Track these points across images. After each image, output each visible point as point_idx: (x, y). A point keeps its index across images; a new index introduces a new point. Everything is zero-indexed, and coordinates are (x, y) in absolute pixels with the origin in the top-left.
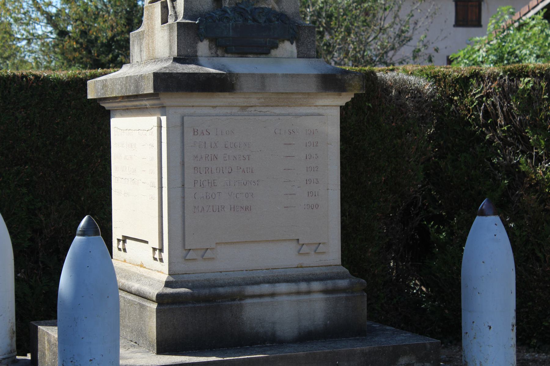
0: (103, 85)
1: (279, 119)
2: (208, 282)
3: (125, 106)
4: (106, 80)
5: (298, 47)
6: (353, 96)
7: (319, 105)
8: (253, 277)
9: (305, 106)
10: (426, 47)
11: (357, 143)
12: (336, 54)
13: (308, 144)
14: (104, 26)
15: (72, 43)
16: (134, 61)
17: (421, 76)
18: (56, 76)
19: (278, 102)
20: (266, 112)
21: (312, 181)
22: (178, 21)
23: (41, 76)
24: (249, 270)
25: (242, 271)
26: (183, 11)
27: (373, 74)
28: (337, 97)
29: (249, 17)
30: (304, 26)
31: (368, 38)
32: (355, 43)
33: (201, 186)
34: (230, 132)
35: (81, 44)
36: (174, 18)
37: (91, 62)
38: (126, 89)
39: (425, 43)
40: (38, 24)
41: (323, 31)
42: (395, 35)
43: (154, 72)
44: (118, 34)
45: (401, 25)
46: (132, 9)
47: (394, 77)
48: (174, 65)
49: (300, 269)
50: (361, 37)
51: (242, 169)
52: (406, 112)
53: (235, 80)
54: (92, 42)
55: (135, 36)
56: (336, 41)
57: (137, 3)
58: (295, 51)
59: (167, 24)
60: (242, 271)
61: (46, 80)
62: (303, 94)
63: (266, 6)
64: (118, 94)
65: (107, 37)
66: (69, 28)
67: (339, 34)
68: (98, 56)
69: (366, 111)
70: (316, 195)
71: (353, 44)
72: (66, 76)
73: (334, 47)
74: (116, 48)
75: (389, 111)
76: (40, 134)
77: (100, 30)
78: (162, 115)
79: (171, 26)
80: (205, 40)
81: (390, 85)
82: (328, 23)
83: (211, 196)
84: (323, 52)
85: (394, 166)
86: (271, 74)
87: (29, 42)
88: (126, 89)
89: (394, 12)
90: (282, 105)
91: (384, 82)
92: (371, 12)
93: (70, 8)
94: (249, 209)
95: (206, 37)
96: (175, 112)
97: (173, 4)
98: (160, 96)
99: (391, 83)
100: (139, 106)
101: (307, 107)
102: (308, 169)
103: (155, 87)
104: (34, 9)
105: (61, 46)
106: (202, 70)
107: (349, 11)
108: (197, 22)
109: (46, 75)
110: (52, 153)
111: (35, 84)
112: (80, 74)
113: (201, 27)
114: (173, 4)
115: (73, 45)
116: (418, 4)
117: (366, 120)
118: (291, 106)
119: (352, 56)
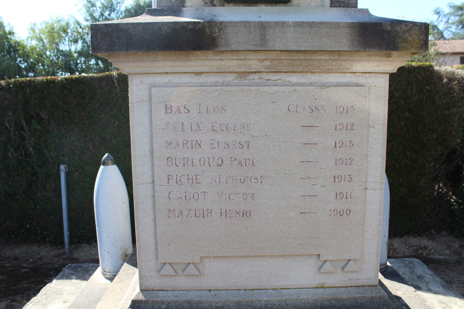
1: (296, 91)
2: (189, 305)
7: (357, 71)
8: (252, 301)
9: (336, 73)
11: (418, 113)
13: (338, 127)
19: (293, 65)
20: (277, 80)
21: (343, 178)
24: (249, 290)
25: (239, 290)
28: (384, 59)
33: (177, 183)
34: (220, 109)
49: (321, 290)
51: (238, 160)
52: (453, 94)
53: (217, 31)
60: (239, 290)
69: (425, 92)
70: (348, 197)
83: (192, 197)
85: (442, 128)
86: (276, 22)
90: (300, 70)
94: (248, 215)
96: (141, 82)
101: (339, 74)
102: (338, 162)
117: (425, 98)
118: (315, 73)
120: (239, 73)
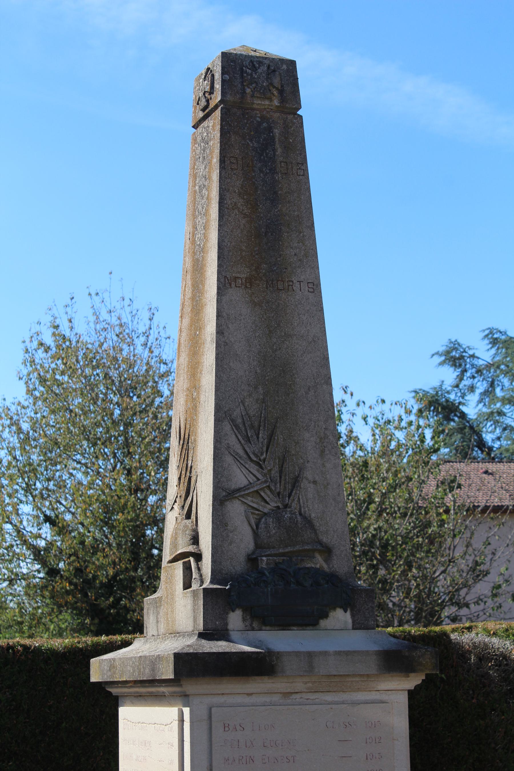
0: (111, 665)
3: (137, 693)
4: (114, 660)
5: (353, 616)
6: (424, 678)
10: (508, 583)
12: (394, 593)
13: (368, 740)
14: (104, 562)
15: (65, 583)
16: (148, 634)
17: (506, 638)
18: (49, 646)
19: (330, 686)
22: (204, 586)
23: (31, 646)
26: (210, 574)
27: (446, 637)
28: (404, 679)
29: (292, 580)
30: (360, 590)
31: (435, 572)
32: (418, 580)
35: (76, 585)
36: (199, 582)
37: (87, 608)
38: (140, 671)
39: (506, 577)
40: (23, 561)
41: (377, 564)
42: (469, 568)
43: (174, 652)
44: (122, 572)
45: (476, 556)
46: (138, 540)
47: (472, 640)
48: (200, 642)
50: (425, 572)
53: (275, 660)
54: (89, 583)
55: (150, 603)
56: (394, 577)
57: (145, 533)
58: (350, 621)
59: (191, 589)
61: (38, 650)
62: (361, 676)
63: (313, 566)
64: (129, 677)
65: (107, 575)
66: (61, 565)
67: (397, 568)
68: (96, 600)
71: (415, 580)
72: (61, 646)
73: (392, 584)
74: (118, 589)
75: (468, 684)
76: (28, 720)
77: (101, 567)
78: (185, 706)
79: (196, 593)
80: (237, 609)
81: (468, 650)
82: (383, 555)
84: (378, 591)
86: (320, 652)
87: (11, 582)
88: (140, 671)
89: (465, 539)
90: (335, 690)
91: (460, 646)
92: (437, 539)
93: (63, 541)
95: (239, 606)
97: (198, 565)
98: (182, 683)
99: (469, 647)
100: (155, 693)
101: (366, 693)
103: (176, 671)
104: (18, 542)
105: (50, 588)
106: (234, 649)
107: (410, 539)
108: (227, 588)
109: (37, 645)
110: (43, 745)
111: (23, 657)
112: (79, 642)
113: (232, 594)
114: (198, 565)
115: (66, 586)
116: (496, 530)
118: (346, 692)
119: (415, 596)
120: (284, 693)
